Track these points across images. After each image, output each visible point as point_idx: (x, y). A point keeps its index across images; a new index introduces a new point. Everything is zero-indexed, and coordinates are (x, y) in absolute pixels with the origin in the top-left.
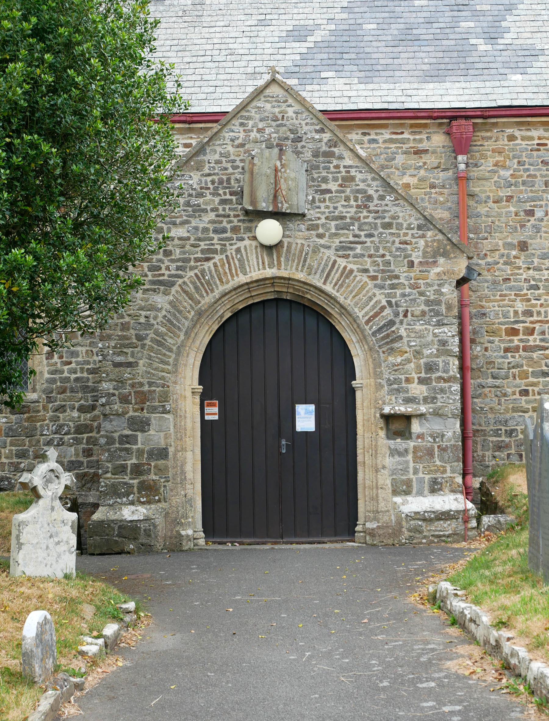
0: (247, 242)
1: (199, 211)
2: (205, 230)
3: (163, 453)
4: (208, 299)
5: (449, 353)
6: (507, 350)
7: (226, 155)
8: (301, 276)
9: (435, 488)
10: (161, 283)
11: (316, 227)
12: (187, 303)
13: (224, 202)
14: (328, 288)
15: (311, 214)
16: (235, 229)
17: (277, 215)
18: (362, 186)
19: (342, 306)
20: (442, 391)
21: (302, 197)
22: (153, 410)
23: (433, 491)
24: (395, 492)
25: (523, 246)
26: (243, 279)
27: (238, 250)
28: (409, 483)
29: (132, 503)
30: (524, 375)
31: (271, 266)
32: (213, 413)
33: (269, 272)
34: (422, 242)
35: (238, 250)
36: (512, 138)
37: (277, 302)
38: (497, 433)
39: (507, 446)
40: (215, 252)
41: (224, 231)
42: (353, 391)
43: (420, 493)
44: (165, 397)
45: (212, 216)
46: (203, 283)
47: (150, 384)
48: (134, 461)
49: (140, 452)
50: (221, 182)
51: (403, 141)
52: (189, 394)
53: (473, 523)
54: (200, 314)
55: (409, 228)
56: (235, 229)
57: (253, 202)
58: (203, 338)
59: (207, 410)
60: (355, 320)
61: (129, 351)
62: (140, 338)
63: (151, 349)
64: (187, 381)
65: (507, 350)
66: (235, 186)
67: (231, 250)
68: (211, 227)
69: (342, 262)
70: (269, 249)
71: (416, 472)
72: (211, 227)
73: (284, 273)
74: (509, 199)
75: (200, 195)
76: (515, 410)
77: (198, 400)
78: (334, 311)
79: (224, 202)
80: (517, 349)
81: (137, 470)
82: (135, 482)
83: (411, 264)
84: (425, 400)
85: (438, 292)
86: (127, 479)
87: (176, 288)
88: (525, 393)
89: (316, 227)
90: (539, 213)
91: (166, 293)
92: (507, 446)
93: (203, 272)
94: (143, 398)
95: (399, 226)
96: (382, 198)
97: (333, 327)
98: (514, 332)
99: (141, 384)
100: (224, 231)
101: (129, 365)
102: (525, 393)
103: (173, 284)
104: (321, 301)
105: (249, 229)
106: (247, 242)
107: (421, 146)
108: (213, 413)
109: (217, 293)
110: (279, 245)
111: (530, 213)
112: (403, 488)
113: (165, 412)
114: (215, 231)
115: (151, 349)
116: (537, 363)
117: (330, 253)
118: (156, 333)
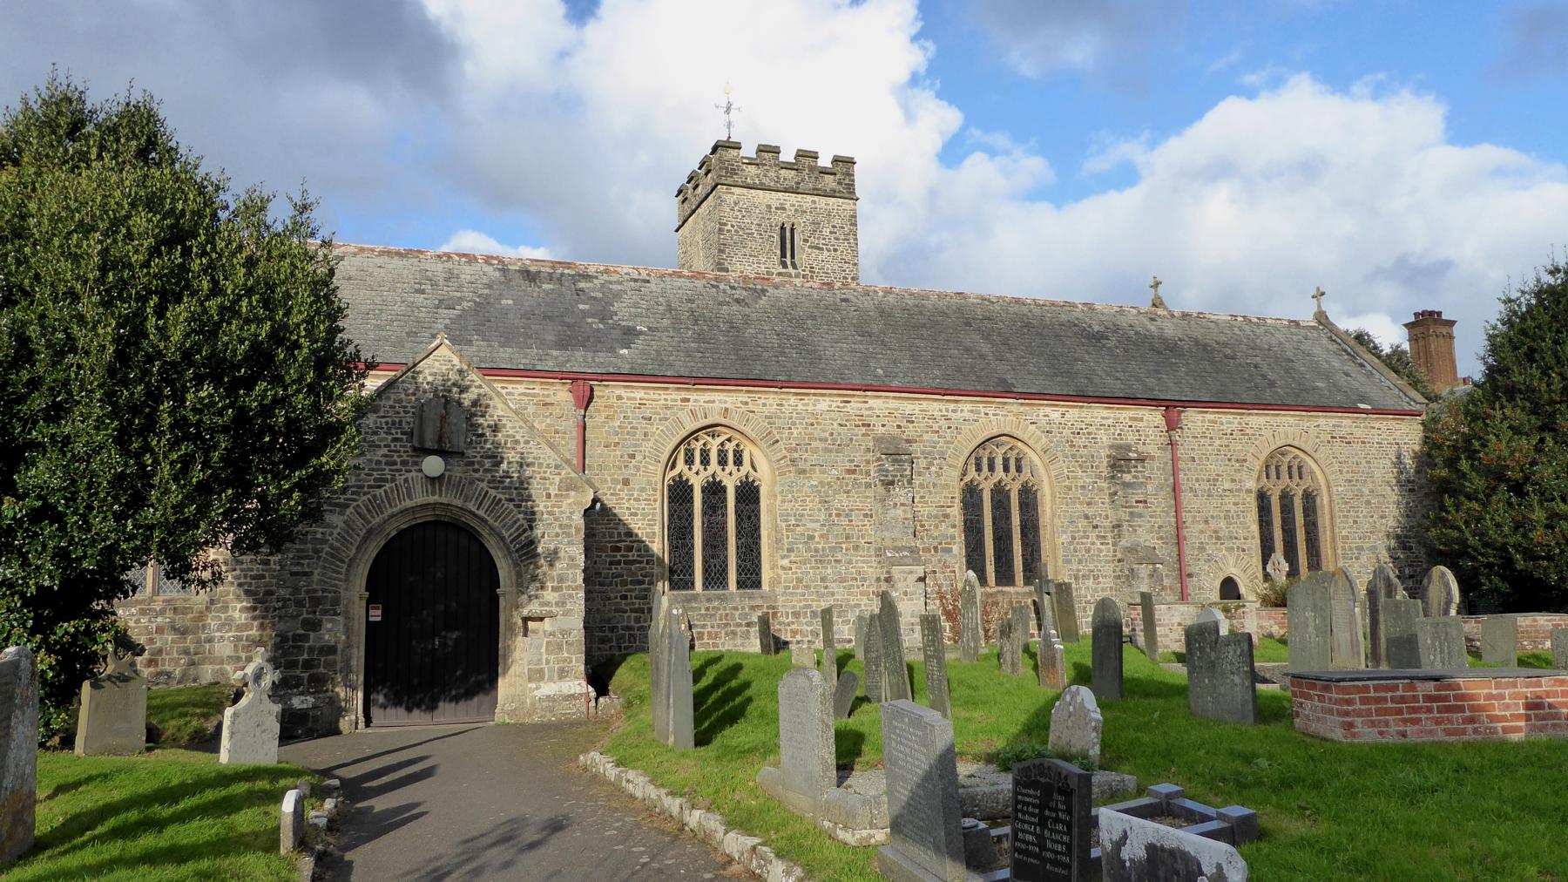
0: (414, 474)
1: (374, 446)
2: (378, 462)
3: (332, 650)
4: (376, 521)
5: (576, 566)
6: (611, 563)
7: (400, 401)
8: (459, 502)
9: (563, 674)
10: (337, 505)
11: (472, 463)
12: (360, 522)
13: (395, 440)
14: (481, 513)
15: (470, 452)
16: (404, 463)
17: (440, 452)
18: (511, 432)
19: (491, 528)
20: (571, 596)
21: (462, 438)
22: (325, 612)
23: (561, 678)
24: (530, 680)
25: (626, 482)
26: (409, 503)
27: (406, 480)
28: (541, 671)
29: (302, 694)
30: (624, 583)
31: (433, 493)
32: (376, 615)
33: (432, 499)
34: (557, 479)
35: (406, 480)
36: (619, 398)
37: (436, 523)
38: (601, 629)
39: (610, 640)
40: (386, 480)
41: (394, 463)
42: (497, 598)
43: (551, 679)
44: (336, 601)
45: (385, 451)
46: (375, 506)
47: (323, 591)
48: (306, 656)
49: (311, 649)
50: (394, 423)
51: (534, 395)
52: (357, 599)
53: (593, 703)
54: (370, 532)
55: (548, 466)
56: (404, 463)
57: (422, 441)
58: (372, 551)
59: (372, 612)
60: (503, 539)
61: (305, 562)
62: (317, 551)
63: (326, 560)
64: (356, 589)
65: (611, 563)
66: (406, 428)
67: (400, 479)
68: (384, 460)
69: (493, 492)
70: (432, 480)
71: (548, 662)
72: (384, 460)
73: (444, 500)
74: (616, 444)
75: (375, 433)
76: (616, 611)
77: (364, 604)
78: (484, 532)
79: (395, 440)
80: (619, 563)
81: (308, 665)
82: (306, 675)
83: (549, 496)
84: (557, 604)
85: (569, 518)
86: (298, 672)
87: (351, 510)
88: (624, 597)
89: (472, 463)
90: (638, 458)
91: (342, 514)
92: (610, 640)
93: (375, 497)
94: (316, 602)
95: (540, 465)
96: (527, 442)
97: (482, 546)
98: (618, 549)
99: (315, 591)
100: (394, 463)
101: (305, 574)
102: (624, 597)
103: (348, 506)
104: (474, 524)
105: (416, 463)
106: (414, 474)
107: (548, 400)
108: (376, 615)
109: (385, 515)
110: (441, 477)
111: (633, 456)
112: (537, 675)
113: (336, 614)
114: (387, 463)
115: (326, 560)
116: (634, 574)
117: (484, 485)
118: (331, 547)
